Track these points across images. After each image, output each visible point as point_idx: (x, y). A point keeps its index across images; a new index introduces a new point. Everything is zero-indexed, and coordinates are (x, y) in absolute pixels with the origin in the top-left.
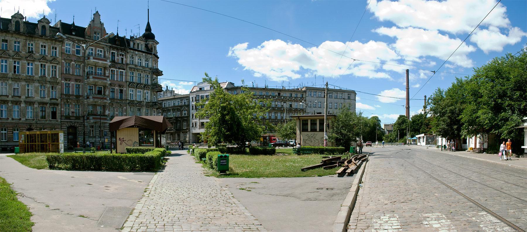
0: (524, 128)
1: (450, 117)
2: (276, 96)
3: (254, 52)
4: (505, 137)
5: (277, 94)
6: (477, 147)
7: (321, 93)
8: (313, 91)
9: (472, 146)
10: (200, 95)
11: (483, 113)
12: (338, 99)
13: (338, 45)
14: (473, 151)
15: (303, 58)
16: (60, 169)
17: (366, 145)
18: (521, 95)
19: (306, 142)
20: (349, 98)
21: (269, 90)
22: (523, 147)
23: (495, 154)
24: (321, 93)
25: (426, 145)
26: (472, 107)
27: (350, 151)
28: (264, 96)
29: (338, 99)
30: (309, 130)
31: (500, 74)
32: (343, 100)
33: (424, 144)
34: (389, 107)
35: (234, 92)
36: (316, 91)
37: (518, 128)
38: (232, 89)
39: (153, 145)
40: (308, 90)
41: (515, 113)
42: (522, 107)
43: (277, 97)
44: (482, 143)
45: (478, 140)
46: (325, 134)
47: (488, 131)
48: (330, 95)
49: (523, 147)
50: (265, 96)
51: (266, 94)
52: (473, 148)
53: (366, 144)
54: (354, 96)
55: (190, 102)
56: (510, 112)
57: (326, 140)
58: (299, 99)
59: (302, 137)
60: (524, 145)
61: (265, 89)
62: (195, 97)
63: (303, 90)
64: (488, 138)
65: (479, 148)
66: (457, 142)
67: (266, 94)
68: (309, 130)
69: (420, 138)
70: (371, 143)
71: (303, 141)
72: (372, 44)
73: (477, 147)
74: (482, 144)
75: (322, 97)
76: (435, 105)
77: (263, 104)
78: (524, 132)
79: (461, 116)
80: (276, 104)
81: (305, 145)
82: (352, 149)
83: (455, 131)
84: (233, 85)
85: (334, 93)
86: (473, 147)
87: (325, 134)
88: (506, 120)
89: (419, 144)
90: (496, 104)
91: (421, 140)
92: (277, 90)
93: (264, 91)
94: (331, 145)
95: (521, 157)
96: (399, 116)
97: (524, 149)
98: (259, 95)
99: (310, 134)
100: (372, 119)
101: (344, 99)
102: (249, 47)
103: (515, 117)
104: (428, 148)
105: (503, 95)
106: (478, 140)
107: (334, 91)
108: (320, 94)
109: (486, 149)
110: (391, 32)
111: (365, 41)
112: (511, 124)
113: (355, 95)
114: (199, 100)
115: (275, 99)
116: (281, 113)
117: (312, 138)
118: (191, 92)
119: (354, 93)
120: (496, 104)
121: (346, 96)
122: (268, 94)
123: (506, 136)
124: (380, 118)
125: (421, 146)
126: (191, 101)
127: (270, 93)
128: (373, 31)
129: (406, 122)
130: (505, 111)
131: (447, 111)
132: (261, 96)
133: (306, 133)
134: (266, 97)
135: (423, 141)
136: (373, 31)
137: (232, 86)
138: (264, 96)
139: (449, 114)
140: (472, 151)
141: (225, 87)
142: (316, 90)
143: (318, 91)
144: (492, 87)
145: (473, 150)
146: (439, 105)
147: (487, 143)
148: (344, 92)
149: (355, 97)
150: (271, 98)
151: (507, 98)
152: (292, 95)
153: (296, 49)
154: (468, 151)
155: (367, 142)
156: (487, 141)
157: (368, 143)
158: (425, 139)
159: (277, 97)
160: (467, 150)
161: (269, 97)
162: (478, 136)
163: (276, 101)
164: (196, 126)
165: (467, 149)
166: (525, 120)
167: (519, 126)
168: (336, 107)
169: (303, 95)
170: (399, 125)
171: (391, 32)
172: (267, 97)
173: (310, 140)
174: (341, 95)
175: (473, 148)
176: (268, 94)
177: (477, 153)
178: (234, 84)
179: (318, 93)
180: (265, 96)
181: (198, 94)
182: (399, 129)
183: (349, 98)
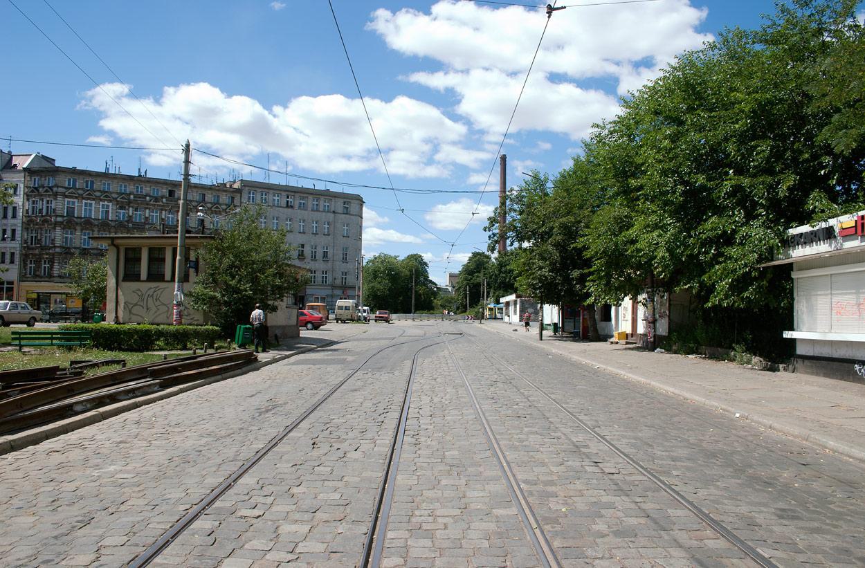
0: (789, 267)
1: (562, 246)
2: (162, 197)
3: (143, 107)
4: (721, 300)
5: (165, 192)
6: (638, 332)
8: (259, 190)
9: (626, 327)
11: (648, 226)
13: (333, 105)
14: (627, 343)
15: (258, 130)
16: (543, 316)
17: (374, 318)
19: (134, 311)
20: (347, 212)
21: (144, 182)
22: (787, 335)
23: (690, 356)
24: (278, 196)
25: (520, 321)
28: (130, 194)
30: (144, 275)
32: (332, 215)
33: (515, 318)
34: (451, 241)
35: (49, 179)
36: (267, 190)
37: (768, 267)
38: (42, 171)
40: (247, 188)
41: (757, 217)
42: (782, 191)
43: (164, 200)
44: (650, 319)
45: (641, 311)
46: (176, 289)
47: (668, 285)
48: (300, 203)
49: (787, 335)
50: (132, 196)
51: (137, 191)
52: (627, 335)
53: (374, 315)
54: (358, 206)
56: (739, 215)
57: (179, 304)
58: (224, 207)
59: (121, 298)
60: (795, 327)
61: (140, 180)
63: (236, 186)
64: (670, 305)
65: (643, 335)
66: (583, 315)
67: (137, 191)
68: (144, 275)
69: (508, 304)
70: (386, 313)
71: (124, 308)
72: (404, 106)
73: (638, 332)
74: (652, 322)
75: (281, 207)
76: (520, 214)
77: (143, 217)
78: (792, 279)
79: (582, 239)
81: (130, 319)
83: (575, 284)
84: (50, 162)
85: (311, 197)
86: (629, 331)
87: (176, 289)
88: (727, 239)
89: (506, 319)
91: (511, 308)
92: (165, 183)
93: (132, 183)
94: (201, 321)
95: (785, 370)
96: (471, 255)
97: (793, 341)
98: (117, 193)
99: (145, 287)
100: (408, 260)
101: (334, 212)
102: (134, 95)
103: (756, 230)
104: (516, 330)
106: (641, 311)
107: (312, 194)
108: (276, 198)
109: (664, 336)
110: (438, 81)
111: (388, 99)
112: (741, 258)
113: (362, 206)
115: (161, 203)
117: (150, 300)
119: (360, 201)
122: (141, 192)
123: (727, 297)
124: (427, 257)
125: (510, 323)
127: (147, 189)
128: (400, 78)
129: (485, 268)
130: (719, 211)
131: (553, 228)
132: (107, 192)
133: (134, 285)
134: (134, 197)
135: (515, 313)
136: (400, 78)
137: (48, 165)
138: (130, 194)
139: (559, 238)
140: (624, 342)
141: (25, 166)
142: (267, 189)
143: (271, 192)
145: (627, 338)
146: (533, 214)
147: (667, 319)
148: (335, 197)
149: (362, 209)
150: (150, 201)
152: (206, 198)
153: (243, 108)
154: (612, 343)
155: (378, 313)
156: (667, 312)
157: (380, 313)
158: (518, 306)
159: (164, 200)
160: (612, 340)
161: (143, 198)
162: (641, 298)
163: (162, 210)
165: (612, 336)
166: (794, 236)
167: (772, 260)
168: (316, 231)
169: (233, 198)
170: (469, 274)
171: (438, 81)
172: (140, 197)
173: (145, 306)
175: (628, 332)
177: (637, 349)
178: (54, 160)
179: (271, 196)
180: (132, 196)
182: (468, 284)
183: (347, 212)
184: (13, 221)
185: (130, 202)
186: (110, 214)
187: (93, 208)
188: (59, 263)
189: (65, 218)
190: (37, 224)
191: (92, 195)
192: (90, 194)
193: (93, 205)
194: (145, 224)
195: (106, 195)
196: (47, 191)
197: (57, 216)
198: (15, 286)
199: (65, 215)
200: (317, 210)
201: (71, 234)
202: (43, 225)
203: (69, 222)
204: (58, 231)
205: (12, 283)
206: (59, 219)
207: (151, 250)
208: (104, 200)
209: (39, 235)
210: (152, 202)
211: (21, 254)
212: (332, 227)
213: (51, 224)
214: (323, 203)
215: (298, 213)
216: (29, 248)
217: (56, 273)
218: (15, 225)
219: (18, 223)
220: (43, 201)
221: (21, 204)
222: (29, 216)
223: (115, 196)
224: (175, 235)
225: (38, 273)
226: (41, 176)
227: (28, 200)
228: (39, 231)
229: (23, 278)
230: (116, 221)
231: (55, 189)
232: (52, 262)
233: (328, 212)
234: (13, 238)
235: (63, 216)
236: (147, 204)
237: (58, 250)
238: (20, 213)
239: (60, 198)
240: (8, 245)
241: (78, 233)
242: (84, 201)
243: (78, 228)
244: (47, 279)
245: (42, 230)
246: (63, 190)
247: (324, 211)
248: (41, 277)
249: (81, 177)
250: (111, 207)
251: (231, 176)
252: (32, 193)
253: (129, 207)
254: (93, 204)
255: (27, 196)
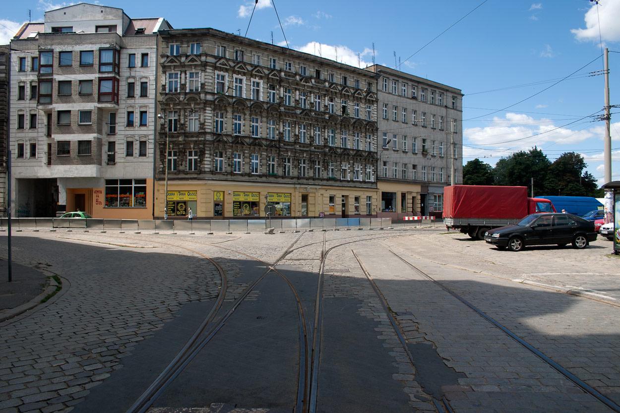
5: (311, 71)
10: (57, 49)
12: (436, 105)
29: (436, 105)
39: (222, 194)
50: (283, 74)
55: (12, 73)
62: (33, 58)
93: (282, 58)
101: (446, 107)
114: (51, 66)
115: (310, 84)
116: (324, 128)
118: (17, 39)
121: (448, 100)
126: (17, 69)
141: (156, 30)
143: (401, 80)
164: (33, 154)
176: (290, 69)
180: (283, 74)
181: (49, 47)
184: (144, 101)
185: (280, 81)
186: (261, 94)
187: (244, 86)
188: (210, 154)
189: (216, 97)
190: (180, 103)
191: (226, 65)
192: (239, 67)
193: (244, 82)
194: (296, 108)
195: (254, 71)
196: (193, 60)
197: (206, 93)
198: (149, 186)
199: (216, 92)
201: (222, 117)
202: (189, 104)
203: (221, 100)
204: (209, 112)
205: (144, 181)
206: (209, 97)
208: (239, 73)
209: (182, 117)
210: (302, 83)
213: (199, 104)
215: (422, 107)
217: (207, 166)
218: (146, 107)
219: (150, 103)
220: (186, 74)
221: (153, 78)
222: (166, 94)
224: (220, 79)
225: (181, 168)
226: (182, 43)
227: (164, 72)
228: (182, 113)
229: (159, 176)
230: (267, 103)
231: (203, 58)
232: (202, 154)
233: (441, 106)
235: (213, 94)
236: (297, 84)
237: (209, 137)
238: (151, 92)
239: (209, 70)
240: (137, 133)
241: (230, 115)
242: (235, 76)
243: (229, 110)
244: (195, 176)
245: (185, 112)
248: (187, 173)
249: (232, 45)
250: (261, 85)
252: (168, 65)
253: (280, 86)
254: (227, 76)
255: (164, 67)
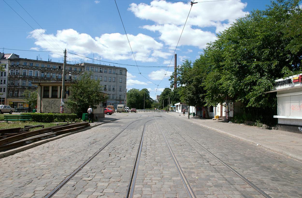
0: (275, 93)
1: (196, 86)
2: (57, 69)
3: (50, 37)
4: (252, 105)
5: (58, 67)
6: (223, 116)
7: (93, 68)
8: (90, 66)
9: (218, 114)
11: (226, 79)
13: (116, 37)
14: (219, 120)
15: (90, 45)
16: (189, 110)
17: (131, 111)
18: (271, 54)
19: (47, 108)
20: (121, 74)
21: (50, 63)
22: (275, 117)
23: (241, 124)
24: (97, 68)
25: (182, 112)
26: (216, 73)
27: (83, 119)
28: (45, 68)
30: (50, 96)
31: (244, 34)
32: (116, 75)
33: (180, 111)
34: (157, 84)
35: (17, 62)
36: (93, 66)
37: (268, 93)
38: (15, 60)
40: (86, 66)
41: (264, 76)
42: (273, 66)
43: (57, 70)
44: (227, 111)
46: (61, 101)
48: (105, 71)
49: (275, 117)
50: (46, 68)
51: (48, 67)
52: (219, 117)
53: (131, 110)
54: (125, 72)
56: (258, 75)
57: (62, 106)
58: (78, 72)
59: (42, 104)
60: (278, 114)
61: (49, 63)
63: (82, 65)
64: (234, 106)
65: (224, 117)
66: (204, 110)
67: (48, 67)
68: (50, 96)
69: (177, 106)
70: (135, 109)
71: (43, 107)
72: (141, 37)
73: (223, 116)
74: (228, 112)
75: (98, 72)
76: (182, 75)
77: (50, 76)
78: (277, 97)
79: (203, 83)
80: (46, 75)
81: (45, 111)
82: (84, 116)
83: (201, 99)
84: (17, 57)
85: (108, 69)
86: (220, 115)
87: (61, 101)
88: (254, 83)
89: (177, 111)
90: (242, 67)
91: (179, 107)
92: (58, 64)
93: (46, 64)
94: (70, 112)
95: (274, 129)
97: (277, 119)
98: (41, 67)
99: (51, 100)
100: (143, 91)
101: (117, 74)
102: (47, 33)
103: (264, 80)
105: (249, 56)
107: (109, 68)
108: (96, 69)
109: (232, 117)
111: (135, 34)
112: (259, 90)
115: (56, 71)
117: (52, 105)
119: (126, 70)
120: (242, 67)
122: (49, 67)
123: (254, 103)
127: (51, 66)
130: (251, 73)
131: (193, 79)
132: (37, 67)
133: (47, 99)
134: (47, 69)
135: (180, 109)
137: (17, 57)
138: (45, 68)
139: (195, 83)
140: (218, 119)
141: (9, 58)
142: (93, 66)
143: (95, 67)
144: (235, 48)
145: (219, 118)
146: (186, 75)
147: (233, 111)
148: (117, 69)
149: (126, 73)
150: (53, 70)
151: (254, 59)
152: (72, 69)
153: (85, 38)
154: (214, 119)
155: (132, 109)
156: (233, 109)
157: (133, 109)
158: (181, 107)
159: (57, 70)
160: (214, 118)
161: (50, 69)
162: (224, 104)
163: (57, 73)
165: (214, 117)
166: (277, 82)
167: (270, 91)
168: (110, 81)
169: (81, 69)
172: (49, 69)
173: (51, 107)
174: (110, 71)
175: (219, 116)
177: (223, 122)
178: (19, 56)
179: (95, 68)
180: (46, 68)
182: (163, 99)
183: (121, 74)
184: (5, 77)
185: (45, 71)
186: (38, 75)
187: (33, 73)
188: (21, 92)
189: (23, 76)
190: (13, 78)
191: (32, 68)
192: (31, 68)
193: (33, 72)
194: (51, 78)
195: (37, 68)
196: (16, 67)
197: (20, 75)
198: (5, 100)
199: (23, 75)
200: (111, 73)
201: (25, 82)
202: (15, 78)
203: (24, 77)
204: (20, 80)
205: (4, 99)
206: (21, 76)
207: (53, 87)
208: (36, 70)
209: (14, 82)
210: (53, 71)
211: (7, 89)
212: (116, 79)
213: (18, 78)
214: (113, 71)
216: (10, 87)
217: (19, 95)
218: (5, 79)
219: (6, 78)
220: (15, 70)
221: (7, 71)
222: (10, 75)
223: (40, 68)
224: (61, 82)
225: (13, 95)
226: (14, 61)
227: (10, 70)
228: (14, 81)
229: (8, 97)
230: (40, 77)
231: (19, 66)
232: (18, 91)
233: (115, 74)
234: (5, 83)
235: (22, 75)
236: (51, 71)
237: (20, 87)
238: (7, 74)
239: (21, 69)
240: (3, 86)
241: (27, 81)
242: (29, 70)
243: (27, 79)
244: (16, 97)
245: (14, 80)
246: (22, 66)
247: (113, 74)
248: (14, 97)
249: (28, 62)
250: (39, 72)
251: (81, 61)
252: (11, 67)
253: (45, 72)
254: (33, 71)
255: (10, 68)
